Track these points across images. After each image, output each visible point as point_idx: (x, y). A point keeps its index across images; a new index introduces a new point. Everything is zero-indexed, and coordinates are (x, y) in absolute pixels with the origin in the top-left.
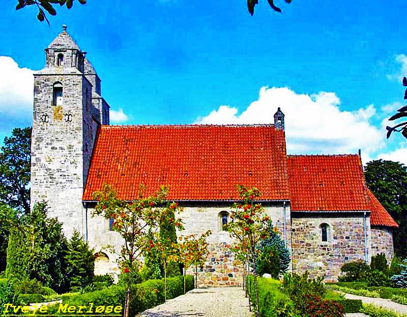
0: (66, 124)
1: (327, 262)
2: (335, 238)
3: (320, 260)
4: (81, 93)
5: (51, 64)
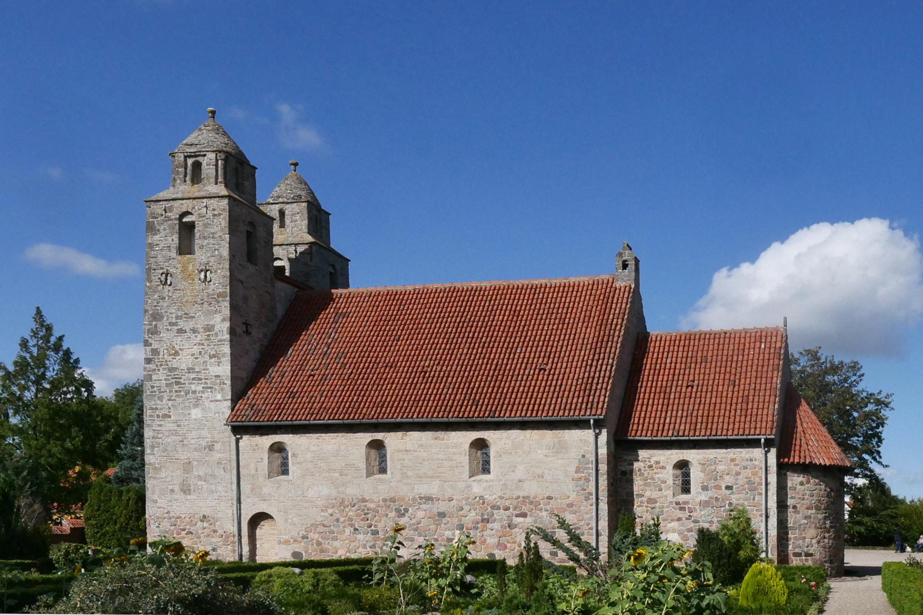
0: (201, 287)
1: (686, 533)
2: (705, 488)
3: (674, 531)
4: (227, 230)
5: (178, 181)
